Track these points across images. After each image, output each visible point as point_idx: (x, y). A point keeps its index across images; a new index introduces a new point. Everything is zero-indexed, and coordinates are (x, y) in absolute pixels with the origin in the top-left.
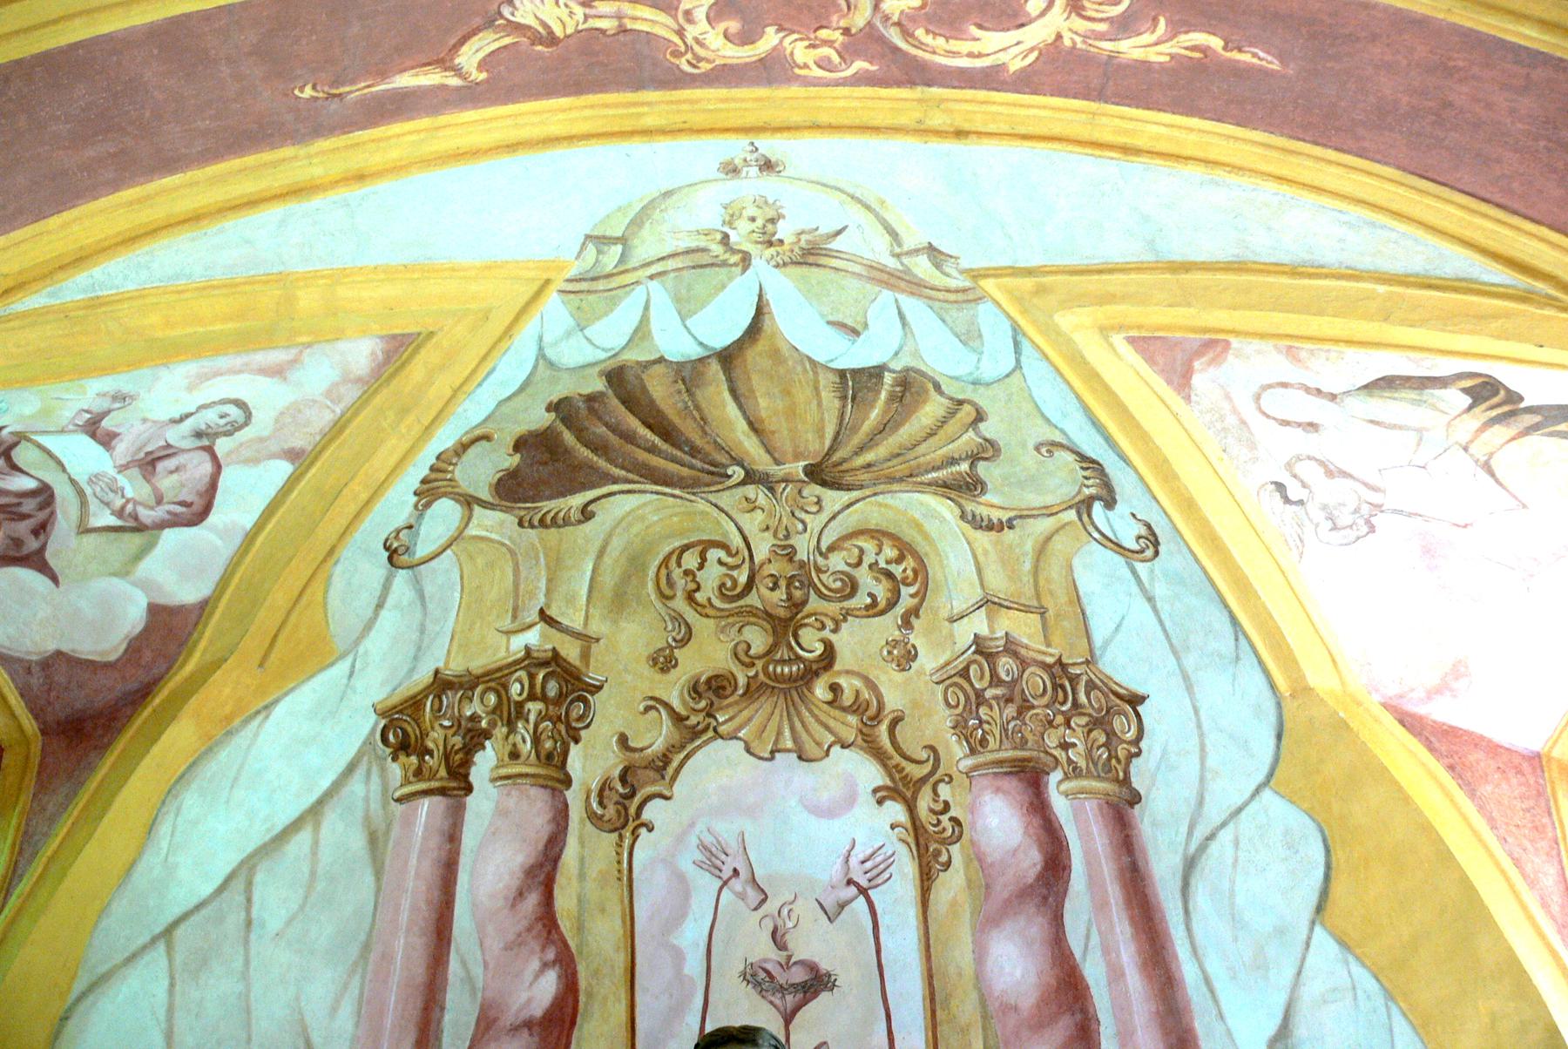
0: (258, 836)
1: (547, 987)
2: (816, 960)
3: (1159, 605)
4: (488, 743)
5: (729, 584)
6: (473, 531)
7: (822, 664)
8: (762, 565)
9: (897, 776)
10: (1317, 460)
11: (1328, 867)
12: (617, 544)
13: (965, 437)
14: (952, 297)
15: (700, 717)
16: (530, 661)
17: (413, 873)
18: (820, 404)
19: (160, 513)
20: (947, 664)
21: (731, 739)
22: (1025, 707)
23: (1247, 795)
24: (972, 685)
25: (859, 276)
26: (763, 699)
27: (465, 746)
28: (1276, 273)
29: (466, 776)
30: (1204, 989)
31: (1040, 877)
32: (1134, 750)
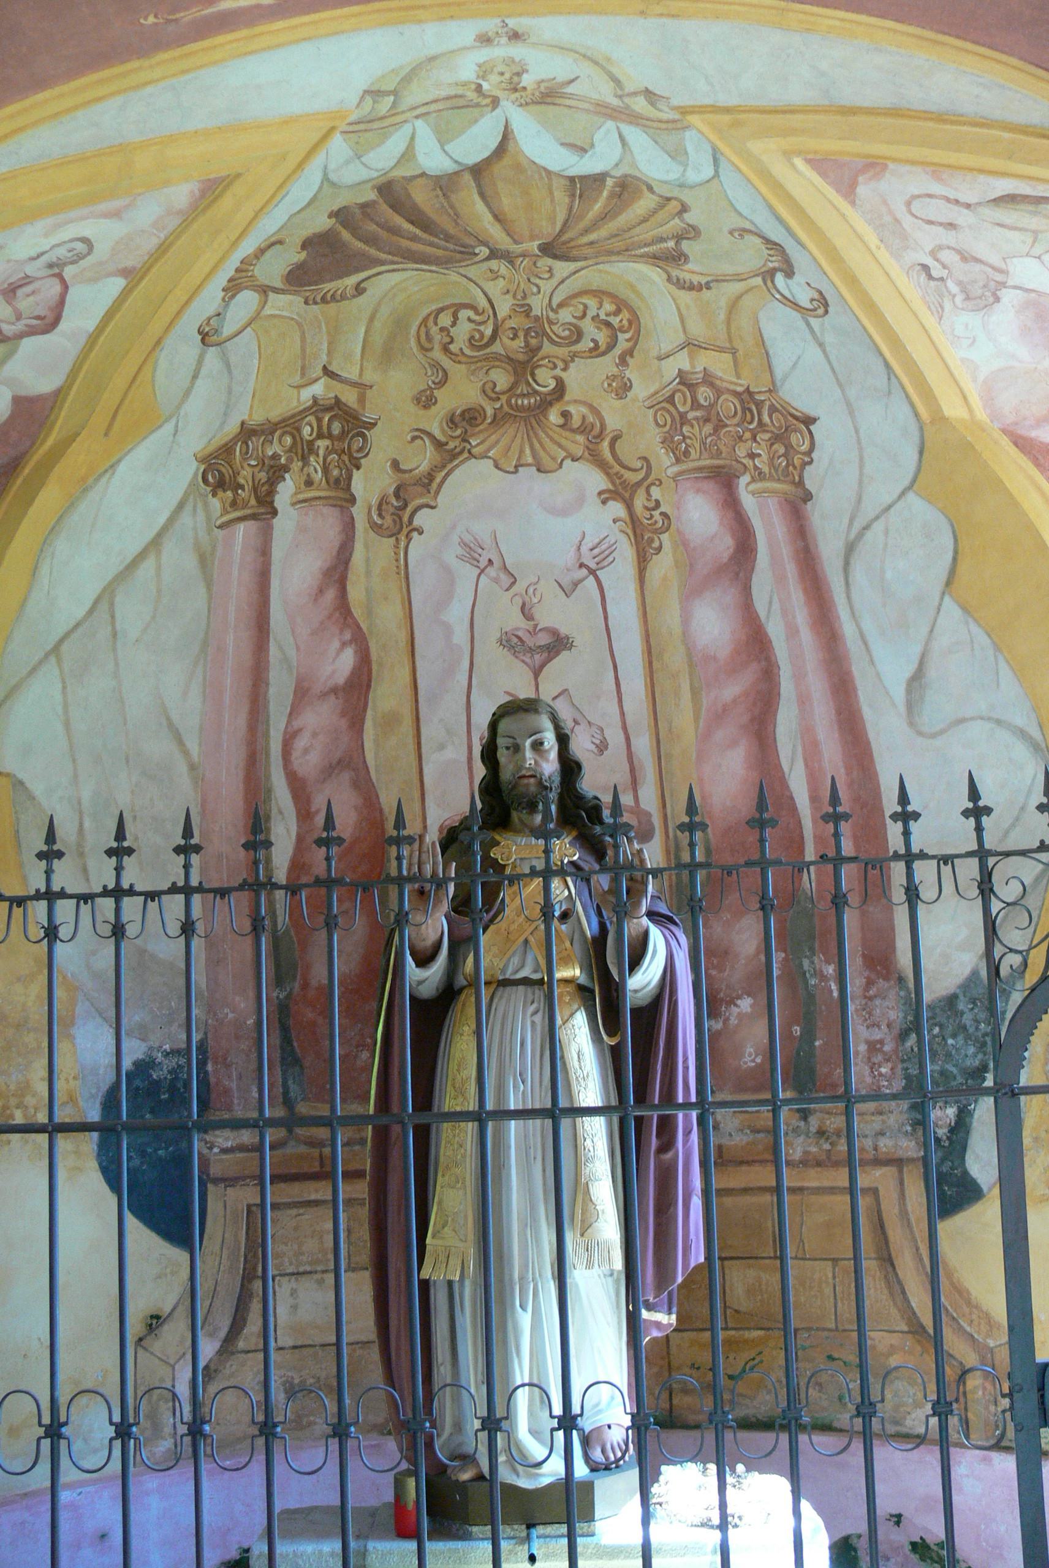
0: (115, 566)
1: (347, 660)
2: (557, 626)
3: (828, 349)
4: (287, 476)
5: (477, 336)
6: (268, 311)
7: (554, 397)
8: (503, 321)
9: (618, 481)
10: (954, 249)
11: (956, 552)
12: (384, 311)
13: (672, 223)
14: (664, 126)
15: (457, 442)
16: (317, 407)
17: (235, 583)
18: (552, 201)
19: (20, 326)
20: (656, 393)
21: (482, 458)
22: (720, 425)
23: (895, 496)
24: (676, 408)
25: (587, 111)
26: (507, 425)
27: (269, 479)
28: (926, 119)
29: (272, 502)
30: (860, 643)
31: (732, 558)
32: (807, 459)
